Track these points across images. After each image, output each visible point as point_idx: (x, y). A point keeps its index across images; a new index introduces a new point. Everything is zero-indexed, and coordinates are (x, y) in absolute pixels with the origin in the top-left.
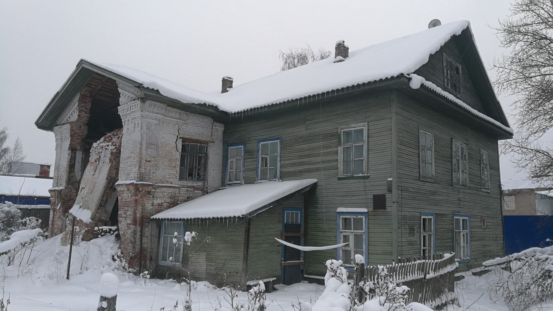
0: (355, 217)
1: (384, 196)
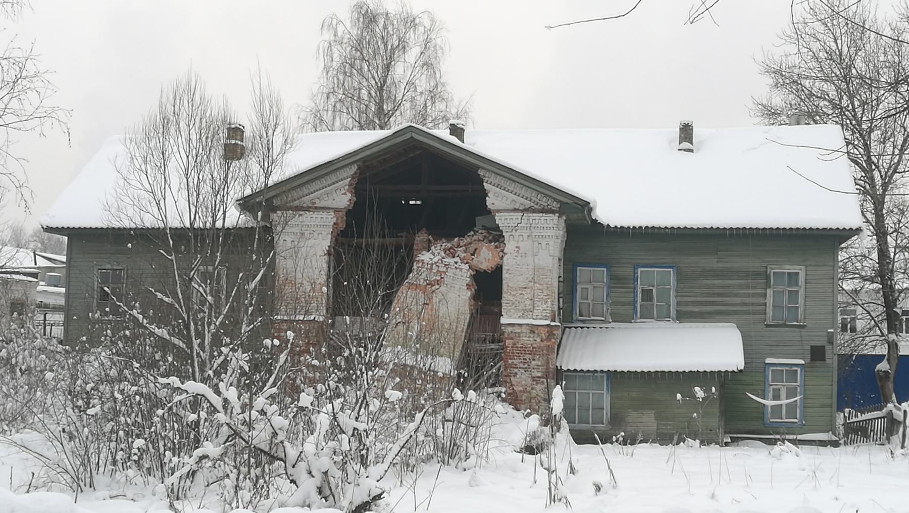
0: (788, 368)
1: (823, 347)
